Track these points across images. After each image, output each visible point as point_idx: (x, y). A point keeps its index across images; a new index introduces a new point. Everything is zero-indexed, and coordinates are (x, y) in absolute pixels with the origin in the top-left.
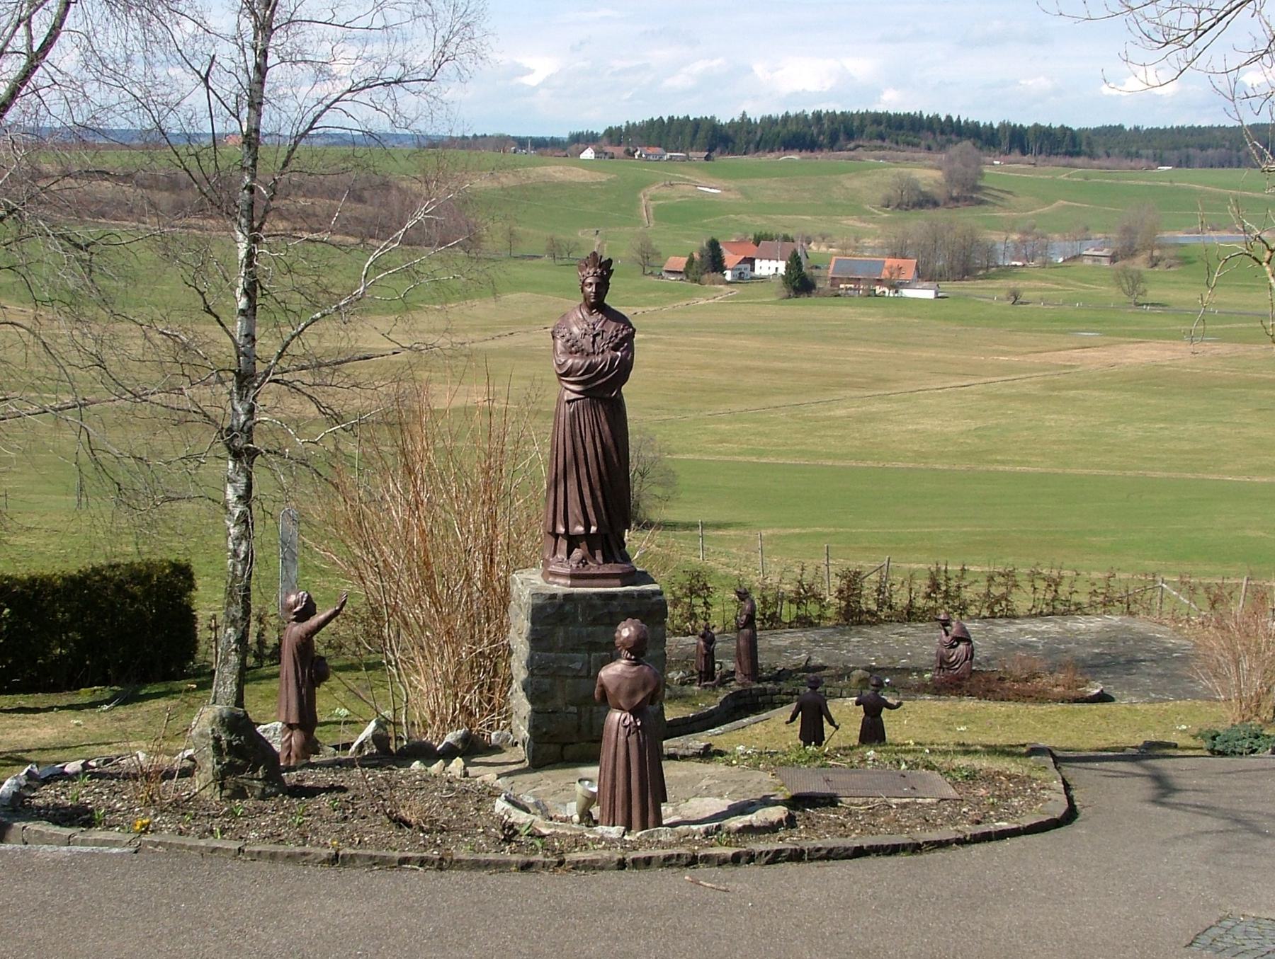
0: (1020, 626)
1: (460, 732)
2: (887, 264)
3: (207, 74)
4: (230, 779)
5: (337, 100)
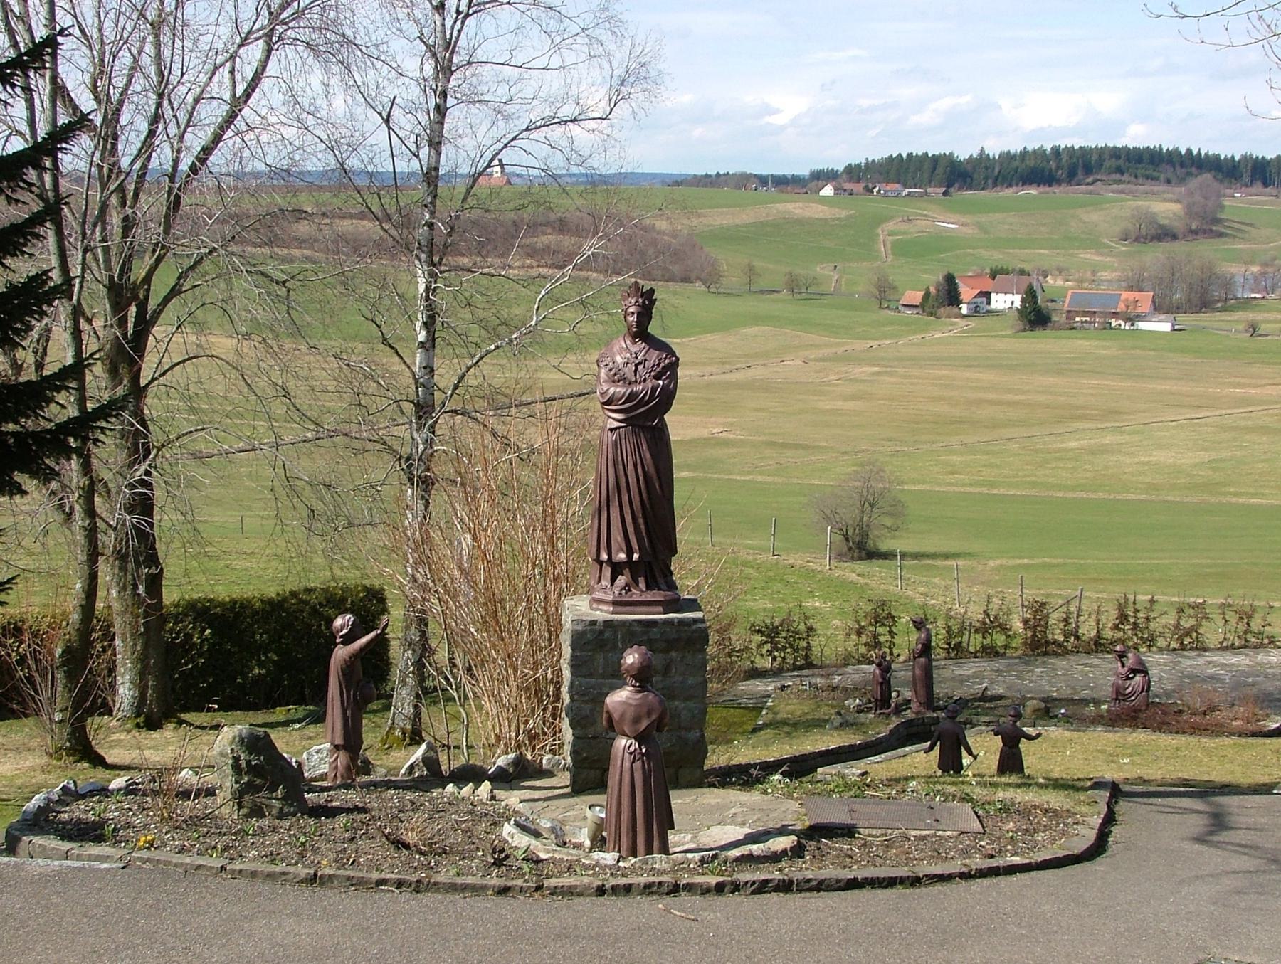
0: (1209, 659)
1: (512, 756)
2: (1123, 297)
3: (389, 115)
4: (248, 798)
5: (514, 139)
